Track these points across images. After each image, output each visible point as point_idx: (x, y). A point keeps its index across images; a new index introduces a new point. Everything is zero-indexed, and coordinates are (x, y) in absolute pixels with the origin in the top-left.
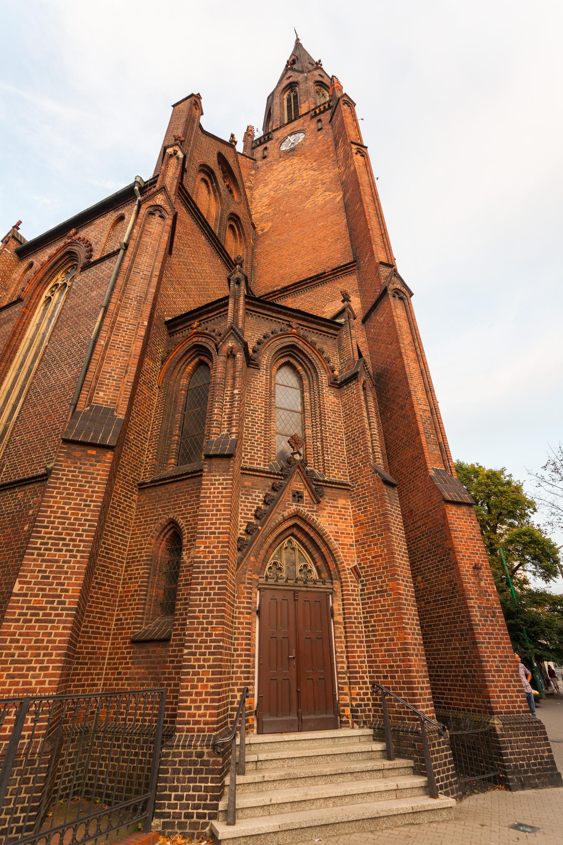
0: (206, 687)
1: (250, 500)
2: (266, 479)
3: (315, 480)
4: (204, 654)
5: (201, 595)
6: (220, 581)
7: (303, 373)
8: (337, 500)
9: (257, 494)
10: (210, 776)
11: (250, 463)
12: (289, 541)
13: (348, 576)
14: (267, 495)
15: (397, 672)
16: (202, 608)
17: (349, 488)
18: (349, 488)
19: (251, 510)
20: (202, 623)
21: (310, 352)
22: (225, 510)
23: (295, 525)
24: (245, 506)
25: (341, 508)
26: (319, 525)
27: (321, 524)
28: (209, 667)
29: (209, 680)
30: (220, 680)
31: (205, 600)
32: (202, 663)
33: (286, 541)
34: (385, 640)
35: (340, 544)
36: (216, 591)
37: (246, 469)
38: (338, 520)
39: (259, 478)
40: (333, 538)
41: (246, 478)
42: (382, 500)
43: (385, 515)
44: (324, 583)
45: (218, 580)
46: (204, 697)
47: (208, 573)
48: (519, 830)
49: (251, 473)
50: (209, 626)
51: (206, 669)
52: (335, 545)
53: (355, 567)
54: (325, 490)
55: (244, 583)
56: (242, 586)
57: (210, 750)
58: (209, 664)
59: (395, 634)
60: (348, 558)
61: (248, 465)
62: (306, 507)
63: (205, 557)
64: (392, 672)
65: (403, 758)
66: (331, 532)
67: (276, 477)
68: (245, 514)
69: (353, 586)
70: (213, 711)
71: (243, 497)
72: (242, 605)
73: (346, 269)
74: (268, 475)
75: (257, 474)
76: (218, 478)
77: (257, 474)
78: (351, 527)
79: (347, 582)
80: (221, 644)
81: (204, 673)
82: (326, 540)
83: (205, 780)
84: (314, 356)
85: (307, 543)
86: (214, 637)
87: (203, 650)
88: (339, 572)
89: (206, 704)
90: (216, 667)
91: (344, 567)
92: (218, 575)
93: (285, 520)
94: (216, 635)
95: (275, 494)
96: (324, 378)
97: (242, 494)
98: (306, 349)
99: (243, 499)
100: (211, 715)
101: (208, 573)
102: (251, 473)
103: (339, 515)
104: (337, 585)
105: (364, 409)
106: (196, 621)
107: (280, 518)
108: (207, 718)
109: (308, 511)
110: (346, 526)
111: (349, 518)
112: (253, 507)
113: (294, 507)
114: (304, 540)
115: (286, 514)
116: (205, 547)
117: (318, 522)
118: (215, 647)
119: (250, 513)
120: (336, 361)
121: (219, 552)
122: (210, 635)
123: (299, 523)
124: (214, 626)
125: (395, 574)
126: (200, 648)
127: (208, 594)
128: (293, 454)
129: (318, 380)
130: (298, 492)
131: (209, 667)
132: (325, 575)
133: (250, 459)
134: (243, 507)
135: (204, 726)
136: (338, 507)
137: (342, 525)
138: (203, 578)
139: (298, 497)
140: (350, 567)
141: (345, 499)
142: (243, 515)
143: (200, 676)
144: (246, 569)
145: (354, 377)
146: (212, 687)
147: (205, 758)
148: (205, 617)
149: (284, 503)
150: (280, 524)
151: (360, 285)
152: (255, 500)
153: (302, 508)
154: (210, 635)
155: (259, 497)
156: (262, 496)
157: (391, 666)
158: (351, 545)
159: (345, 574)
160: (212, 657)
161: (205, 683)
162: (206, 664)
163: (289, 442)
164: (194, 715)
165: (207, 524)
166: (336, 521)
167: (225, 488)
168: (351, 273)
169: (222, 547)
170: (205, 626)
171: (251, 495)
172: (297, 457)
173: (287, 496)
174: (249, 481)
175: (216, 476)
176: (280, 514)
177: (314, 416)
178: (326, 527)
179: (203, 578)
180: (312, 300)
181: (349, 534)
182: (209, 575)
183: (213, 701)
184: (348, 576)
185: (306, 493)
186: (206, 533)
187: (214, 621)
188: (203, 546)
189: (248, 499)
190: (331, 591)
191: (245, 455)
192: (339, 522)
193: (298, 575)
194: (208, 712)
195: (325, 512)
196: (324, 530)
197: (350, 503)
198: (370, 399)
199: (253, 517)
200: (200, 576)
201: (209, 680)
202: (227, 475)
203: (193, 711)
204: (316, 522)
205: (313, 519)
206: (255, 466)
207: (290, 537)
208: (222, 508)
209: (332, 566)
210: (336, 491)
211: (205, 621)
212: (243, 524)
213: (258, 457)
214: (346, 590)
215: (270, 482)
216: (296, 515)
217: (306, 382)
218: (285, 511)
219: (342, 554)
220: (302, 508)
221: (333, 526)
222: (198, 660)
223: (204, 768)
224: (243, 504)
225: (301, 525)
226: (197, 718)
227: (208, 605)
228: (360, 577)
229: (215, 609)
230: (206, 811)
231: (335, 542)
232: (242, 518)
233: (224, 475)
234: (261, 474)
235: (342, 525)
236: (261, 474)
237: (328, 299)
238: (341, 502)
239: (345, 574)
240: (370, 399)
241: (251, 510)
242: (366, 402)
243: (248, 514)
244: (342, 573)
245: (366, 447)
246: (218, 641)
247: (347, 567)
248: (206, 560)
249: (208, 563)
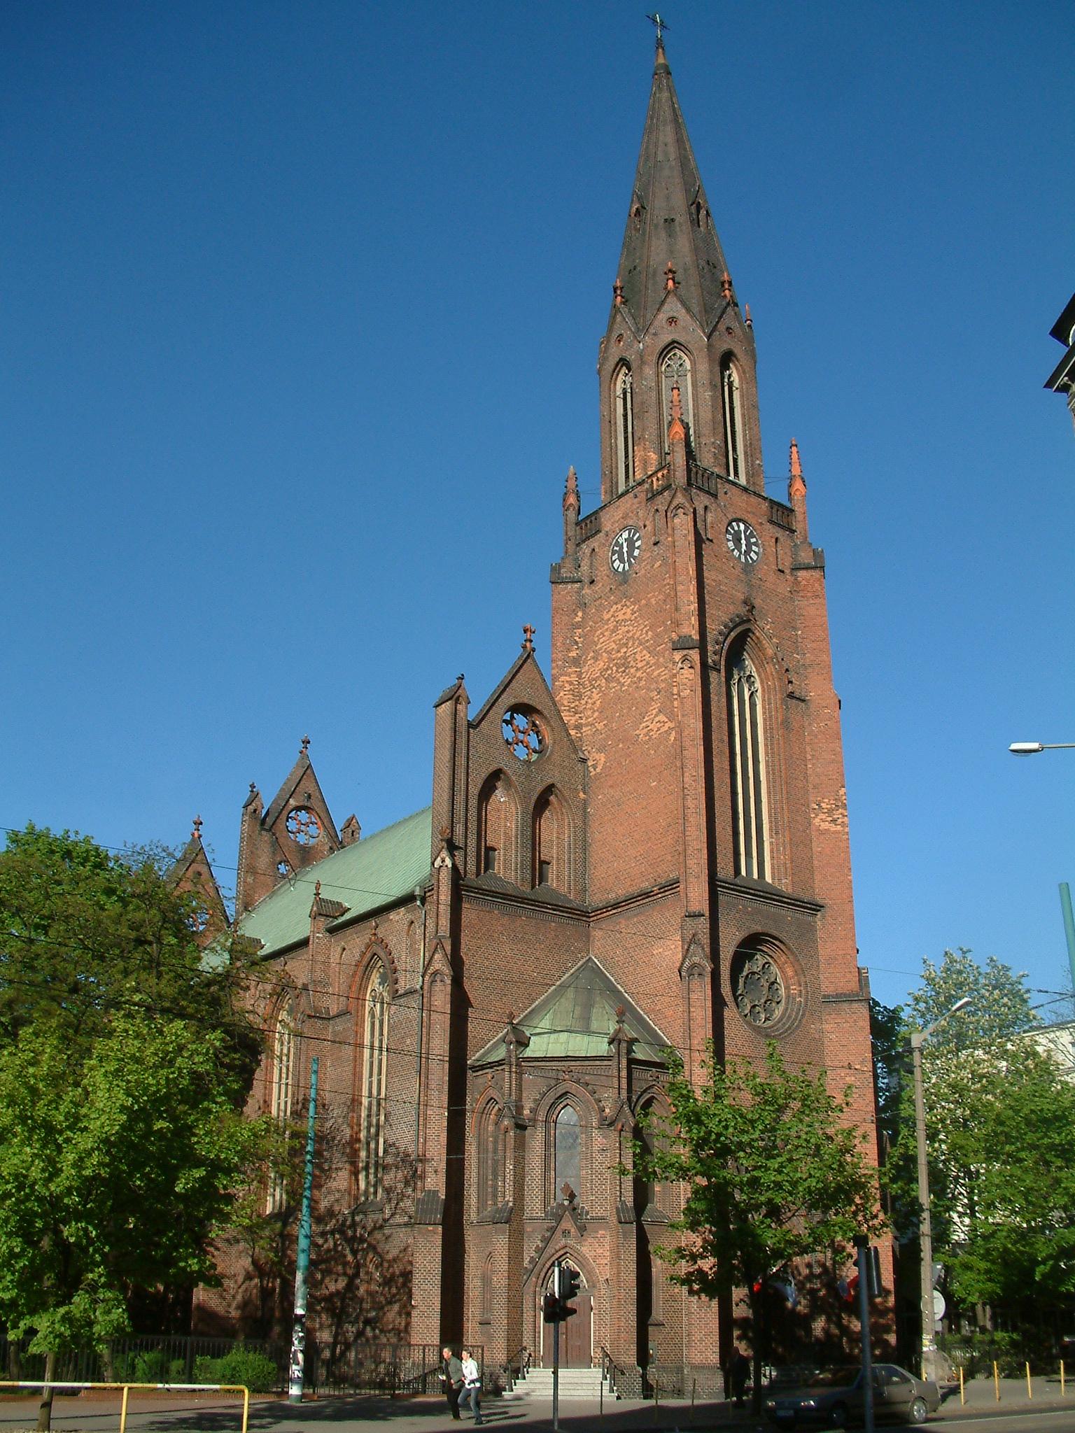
173: (559, 1233)
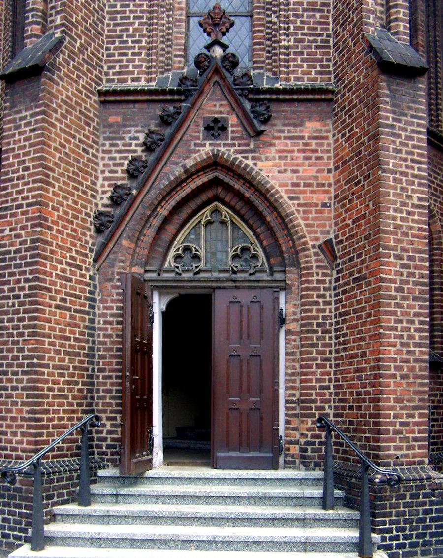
0: (21, 411)
1: (121, 148)
2: (151, 106)
3: (251, 91)
4: (16, 373)
5: (8, 298)
6: (30, 277)
8: (301, 125)
9: (133, 134)
10: (24, 503)
11: (120, 81)
12: (216, 211)
13: (313, 259)
15: (364, 401)
16: (10, 316)
17: (330, 96)
18: (330, 96)
19: (122, 165)
20: (12, 335)
22: (34, 167)
23: (215, 182)
24: (111, 158)
25: (310, 138)
26: (258, 174)
27: (264, 174)
28: (23, 389)
29: (23, 404)
30: (36, 404)
31: (14, 305)
32: (15, 384)
33: (207, 210)
34: (356, 355)
35: (299, 205)
36: (27, 292)
37: (107, 93)
38: (300, 161)
39: (137, 106)
40: (285, 197)
41: (112, 109)
45: (28, 276)
46: (19, 422)
47: (16, 266)
49: (118, 98)
50: (21, 339)
51: (20, 392)
52: (290, 207)
53: (329, 243)
54: (274, 107)
55: (111, 280)
56: (109, 285)
57: (21, 478)
58: (22, 385)
59: (368, 346)
61: (114, 86)
62: (234, 145)
63: (11, 245)
64: (358, 400)
65: (352, 508)
66: (281, 185)
67: (169, 97)
68: (111, 172)
70: (30, 439)
71: (107, 143)
72: (109, 312)
74: (154, 97)
75: (131, 98)
76: (24, 114)
77: (131, 98)
78: (330, 171)
79: (311, 268)
80: (35, 361)
81: (18, 396)
82: (272, 200)
83: (19, 506)
86: (26, 353)
87: (15, 369)
88: (297, 253)
89: (22, 430)
90: (31, 388)
91: (306, 243)
92: (28, 269)
93: (190, 174)
94: (29, 350)
97: (105, 139)
99: (107, 148)
100: (28, 443)
101: (16, 266)
102: (118, 98)
103: (304, 151)
104: (292, 276)
106: (5, 332)
107: (178, 171)
108: (25, 446)
109: (237, 152)
110: (318, 171)
111: (325, 156)
112: (126, 158)
113: (208, 148)
115: (190, 163)
116: (11, 230)
117: (257, 169)
118: (28, 365)
119: (119, 169)
121: (27, 235)
122: (21, 350)
123: (222, 176)
124: (26, 338)
125: (379, 246)
126: (12, 366)
127: (17, 297)
128: (209, 47)
130: (216, 120)
131: (23, 389)
133: (119, 73)
134: (106, 161)
135: (22, 454)
136: (302, 138)
138: (11, 275)
139: (216, 128)
140: (317, 244)
141: (321, 119)
142: (107, 174)
143: (14, 400)
144: (115, 260)
146: (28, 412)
147: (18, 485)
148: (16, 328)
149: (187, 143)
150: (179, 183)
152: (130, 145)
153: (223, 149)
154: (21, 350)
155: (137, 139)
156: (142, 137)
157: (359, 393)
158: (324, 205)
159: (306, 256)
160: (25, 377)
161: (19, 407)
162: (20, 385)
163: (201, 25)
164: (11, 442)
165: (11, 194)
167: (34, 130)
169: (33, 226)
170: (16, 338)
171: (122, 139)
172: (218, 52)
173: (194, 129)
174: (117, 114)
175: (20, 112)
176: (177, 164)
178: (273, 178)
179: (11, 275)
181: (323, 185)
182: (17, 270)
183: (29, 427)
184: (313, 259)
185: (233, 120)
186: (11, 208)
187: (26, 331)
188: (8, 228)
189: (117, 145)
190: (282, 284)
191: (110, 68)
192: (302, 165)
194: (25, 439)
195: (273, 149)
196: (268, 182)
197: (331, 127)
199: (126, 175)
200: (7, 272)
201: (23, 404)
202: (37, 107)
203: (9, 437)
204: (252, 169)
205: (247, 166)
206: (129, 85)
207: (216, 203)
208: (31, 165)
210: (300, 108)
211: (15, 332)
212: (107, 188)
213: (135, 67)
214: (306, 282)
215: (158, 110)
216: (214, 163)
218: (188, 157)
219: (302, 223)
220: (223, 149)
221: (289, 174)
222: (10, 381)
223: (17, 494)
224: (107, 156)
225: (227, 179)
226: (14, 445)
227: (18, 312)
228: (335, 258)
229: (26, 316)
230: (21, 534)
231: (290, 203)
232: (105, 179)
233: (31, 108)
234: (140, 98)
236: (140, 98)
238: (311, 126)
239: (306, 256)
241: (122, 165)
243: (116, 172)
244: (301, 254)
246: (32, 357)
247: (310, 243)
248: (13, 249)
249: (15, 252)
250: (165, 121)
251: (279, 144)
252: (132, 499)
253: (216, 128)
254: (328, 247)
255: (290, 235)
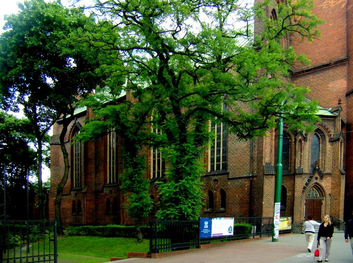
7: (320, 137)
14: (308, 179)
21: (324, 130)
42: (340, 179)
43: (340, 182)
44: (321, 197)
48: (255, 98)
52: (325, 189)
60: (328, 191)
69: (328, 198)
73: (343, 62)
84: (325, 131)
85: (318, 189)
95: (310, 179)
96: (327, 139)
98: (324, 132)
105: (340, 151)
114: (317, 188)
115: (313, 183)
120: (332, 133)
129: (325, 140)
132: (321, 196)
137: (328, 184)
139: (316, 178)
145: (338, 140)
151: (348, 73)
156: (307, 180)
166: (326, 184)
168: (344, 65)
173: (314, 178)
177: (322, 152)
180: (323, 78)
184: (328, 196)
185: (319, 177)
193: (315, 196)
198: (343, 146)
209: (324, 194)
215: (309, 176)
216: (316, 183)
217: (321, 140)
235: (328, 184)
237: (331, 79)
238: (328, 178)
240: (343, 146)
242: (341, 147)
245: (338, 164)
250: (310, 177)
251: (324, 181)
252: (215, 242)
253: (316, 178)
254: (330, 194)
255: (324, 192)
